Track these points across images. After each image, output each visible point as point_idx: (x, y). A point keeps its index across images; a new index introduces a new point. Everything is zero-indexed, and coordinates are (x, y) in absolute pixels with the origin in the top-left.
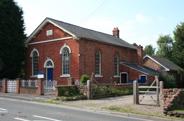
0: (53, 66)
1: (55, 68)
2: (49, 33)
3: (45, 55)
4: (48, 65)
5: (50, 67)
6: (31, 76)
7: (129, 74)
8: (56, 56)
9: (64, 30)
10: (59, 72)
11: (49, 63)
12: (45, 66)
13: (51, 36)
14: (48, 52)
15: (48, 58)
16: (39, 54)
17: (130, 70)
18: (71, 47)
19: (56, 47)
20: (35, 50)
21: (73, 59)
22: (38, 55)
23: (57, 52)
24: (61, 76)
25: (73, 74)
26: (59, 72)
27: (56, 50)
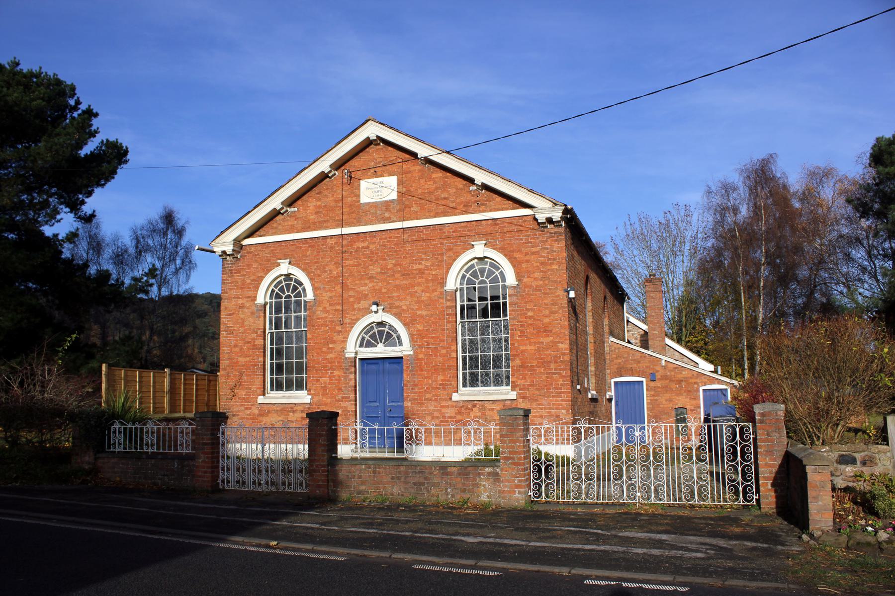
0: (405, 349)
1: (415, 357)
2: (378, 189)
3: (351, 293)
4: (369, 345)
5: (381, 351)
6: (264, 395)
7: (652, 384)
8: (419, 302)
9: (324, 165)
10: (440, 378)
11: (380, 334)
12: (352, 348)
13: (387, 204)
14: (371, 278)
15: (374, 308)
16: (315, 289)
17: (658, 368)
18: (516, 255)
19: (860, 298)
20: (284, 267)
21: (530, 314)
22: (310, 296)
23: (427, 281)
24: (261, 399)
25: (532, 385)
26: (440, 378)
27: (421, 272)
